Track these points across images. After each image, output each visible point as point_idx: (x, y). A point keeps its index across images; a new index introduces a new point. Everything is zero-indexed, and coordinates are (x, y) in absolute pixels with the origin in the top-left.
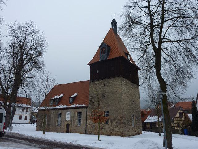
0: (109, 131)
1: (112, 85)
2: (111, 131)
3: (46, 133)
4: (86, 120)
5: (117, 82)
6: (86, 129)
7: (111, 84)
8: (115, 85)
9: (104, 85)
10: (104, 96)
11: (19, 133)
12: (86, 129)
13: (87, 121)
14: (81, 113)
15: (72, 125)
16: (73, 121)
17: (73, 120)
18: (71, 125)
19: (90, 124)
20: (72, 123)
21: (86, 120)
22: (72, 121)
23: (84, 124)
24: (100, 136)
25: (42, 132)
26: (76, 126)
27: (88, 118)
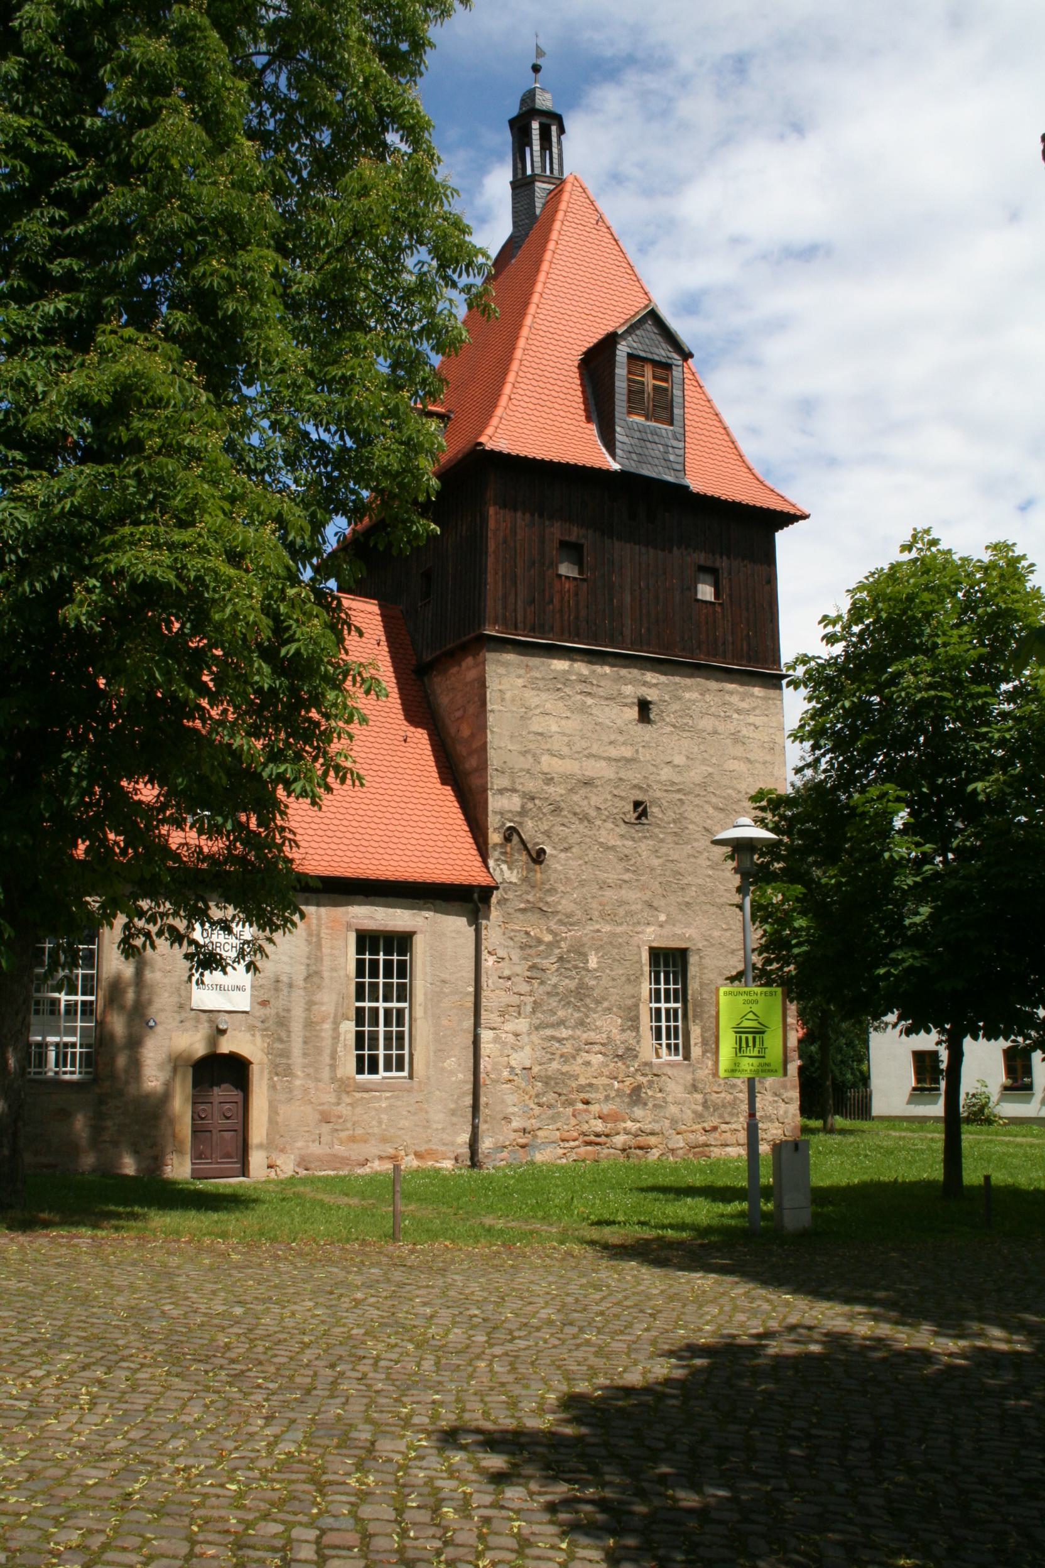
0: (699, 1117)
1: (715, 732)
2: (714, 1121)
3: (982, 1181)
4: (477, 1024)
5: (748, 712)
6: (475, 1107)
7: (707, 723)
8: (737, 738)
9: (644, 707)
10: (641, 810)
11: (443, 461)
12: (475, 1107)
13: (486, 1035)
14: (401, 942)
15: (288, 1072)
16: (309, 1024)
17: (298, 1014)
18: (281, 1068)
19: (521, 1058)
20: (286, 1054)
21: (477, 1024)
22: (283, 1022)
23: (450, 1063)
24: (937, 1173)
25: (993, 1181)
26: (344, 1087)
27: (492, 998)
